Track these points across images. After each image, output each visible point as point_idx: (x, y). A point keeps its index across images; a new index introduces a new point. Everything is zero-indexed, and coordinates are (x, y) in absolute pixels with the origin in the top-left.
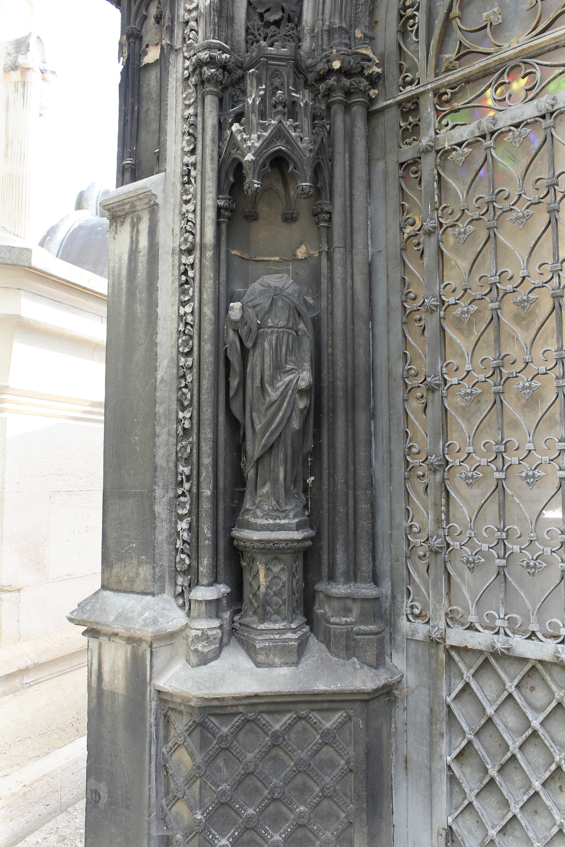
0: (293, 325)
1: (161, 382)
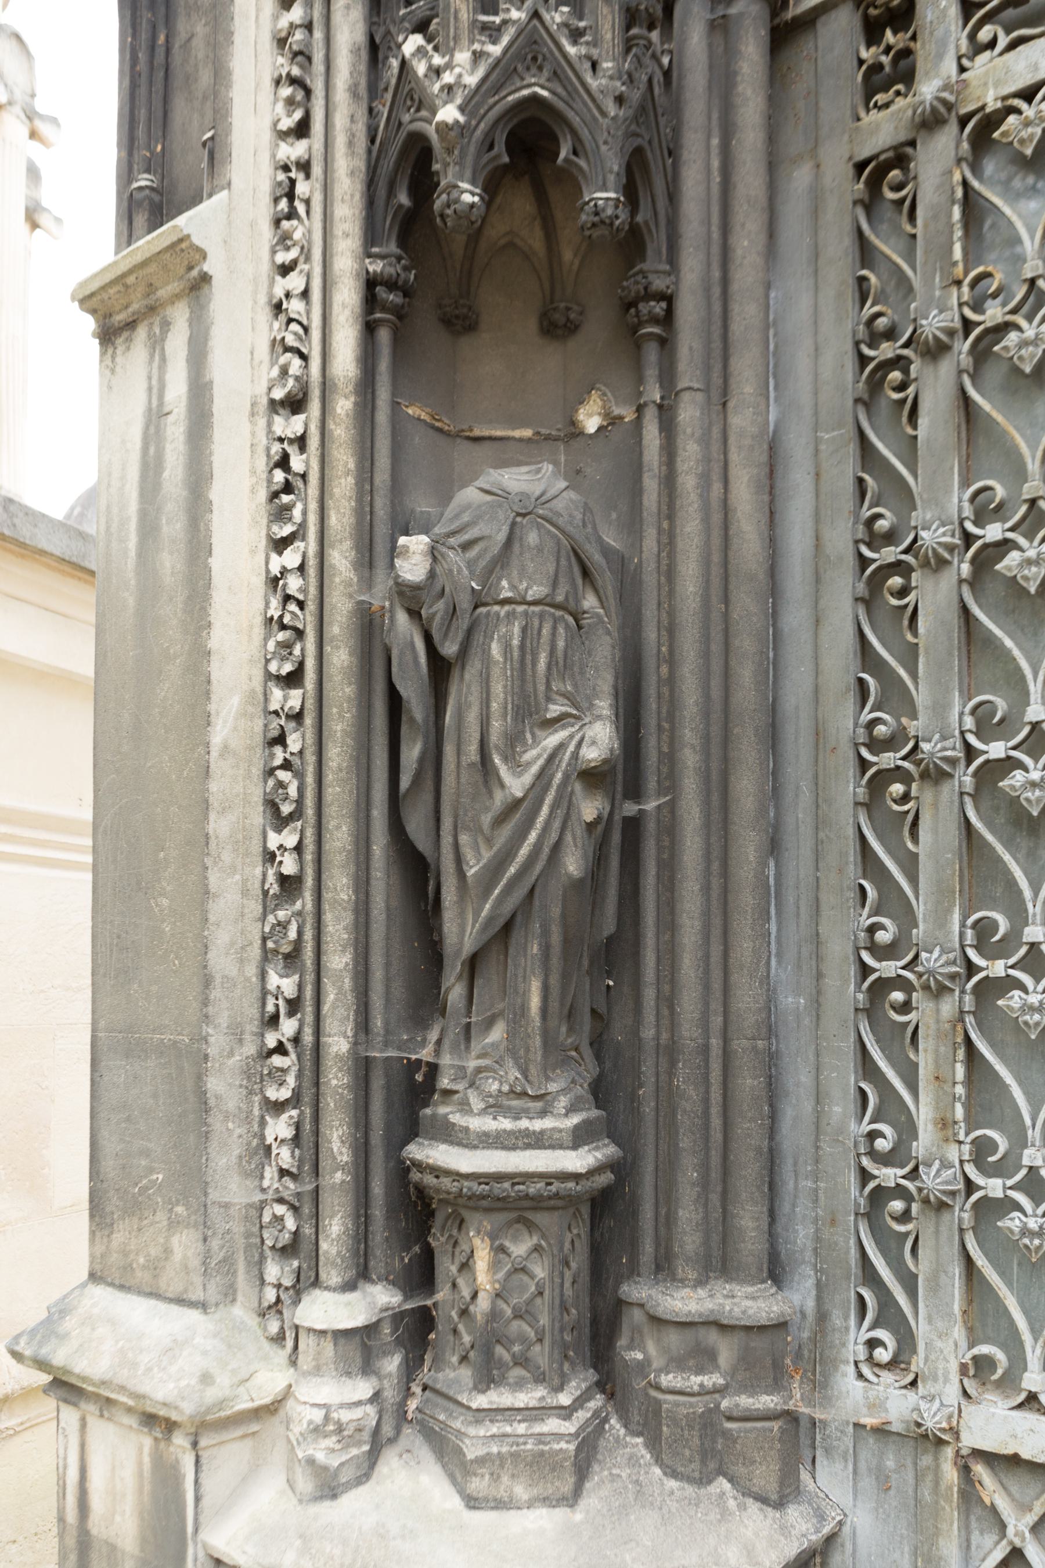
0: (567, 598)
1: (221, 755)
